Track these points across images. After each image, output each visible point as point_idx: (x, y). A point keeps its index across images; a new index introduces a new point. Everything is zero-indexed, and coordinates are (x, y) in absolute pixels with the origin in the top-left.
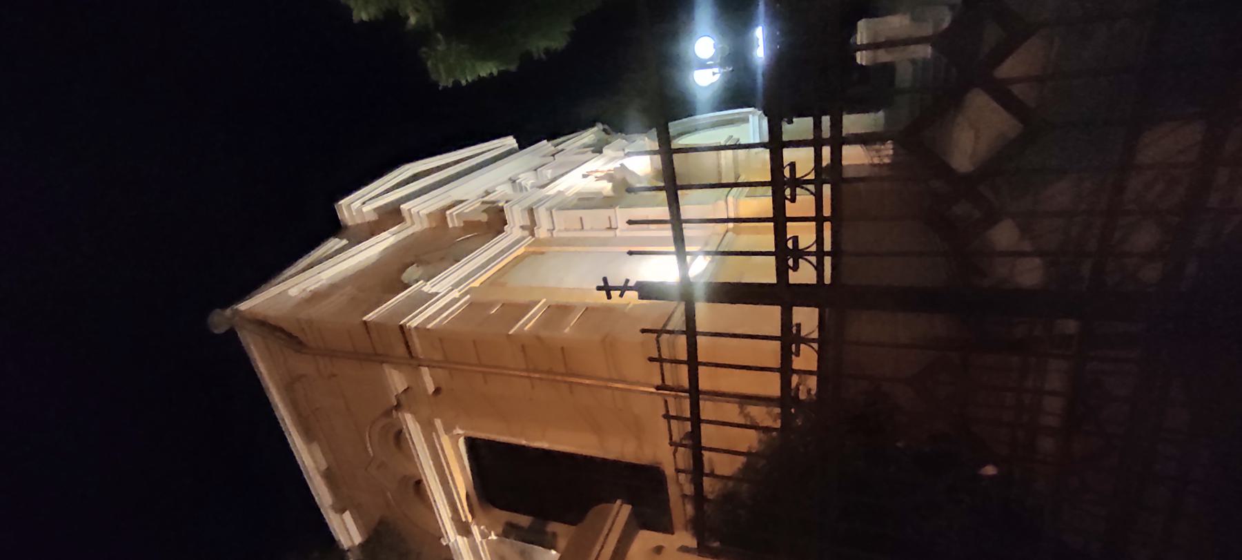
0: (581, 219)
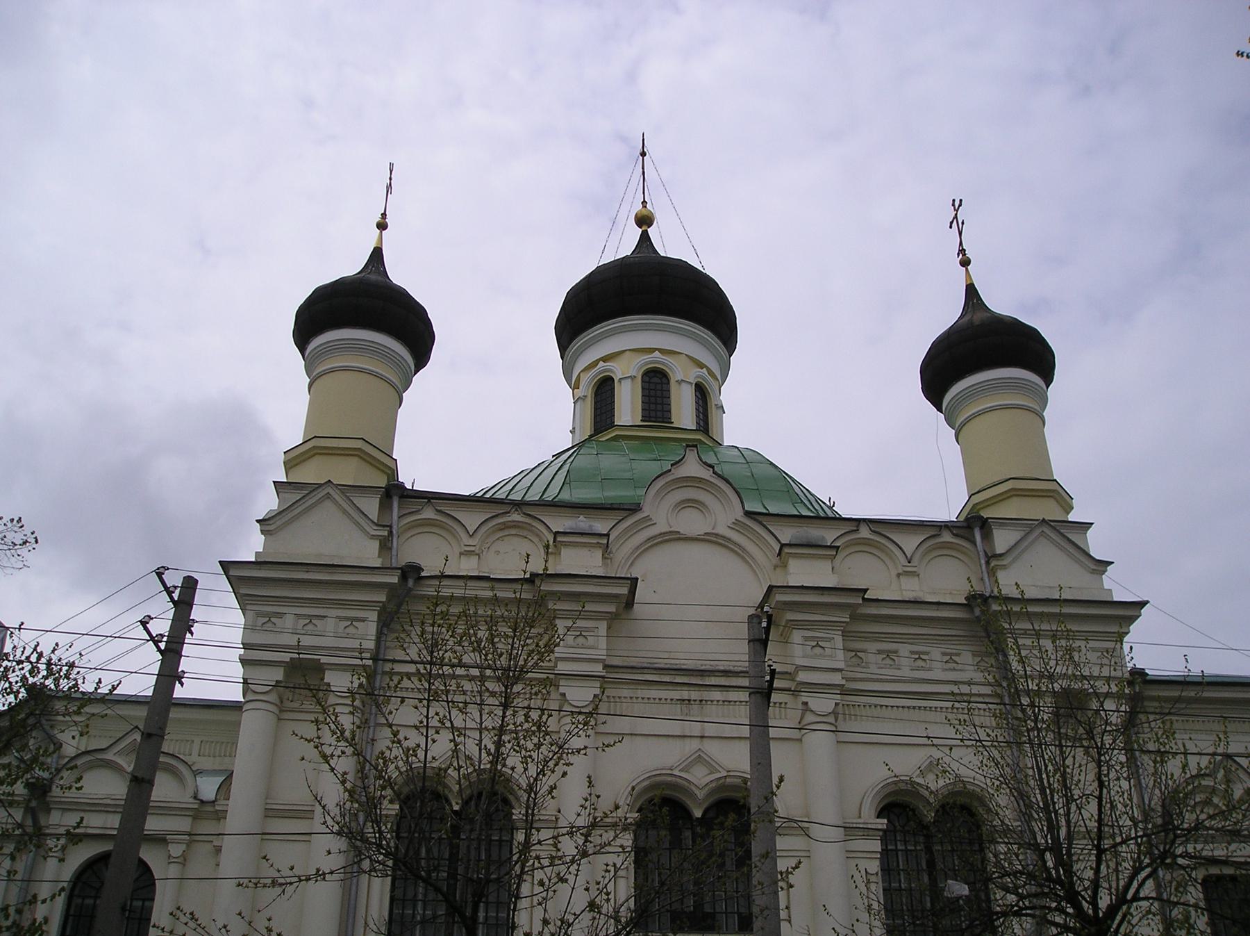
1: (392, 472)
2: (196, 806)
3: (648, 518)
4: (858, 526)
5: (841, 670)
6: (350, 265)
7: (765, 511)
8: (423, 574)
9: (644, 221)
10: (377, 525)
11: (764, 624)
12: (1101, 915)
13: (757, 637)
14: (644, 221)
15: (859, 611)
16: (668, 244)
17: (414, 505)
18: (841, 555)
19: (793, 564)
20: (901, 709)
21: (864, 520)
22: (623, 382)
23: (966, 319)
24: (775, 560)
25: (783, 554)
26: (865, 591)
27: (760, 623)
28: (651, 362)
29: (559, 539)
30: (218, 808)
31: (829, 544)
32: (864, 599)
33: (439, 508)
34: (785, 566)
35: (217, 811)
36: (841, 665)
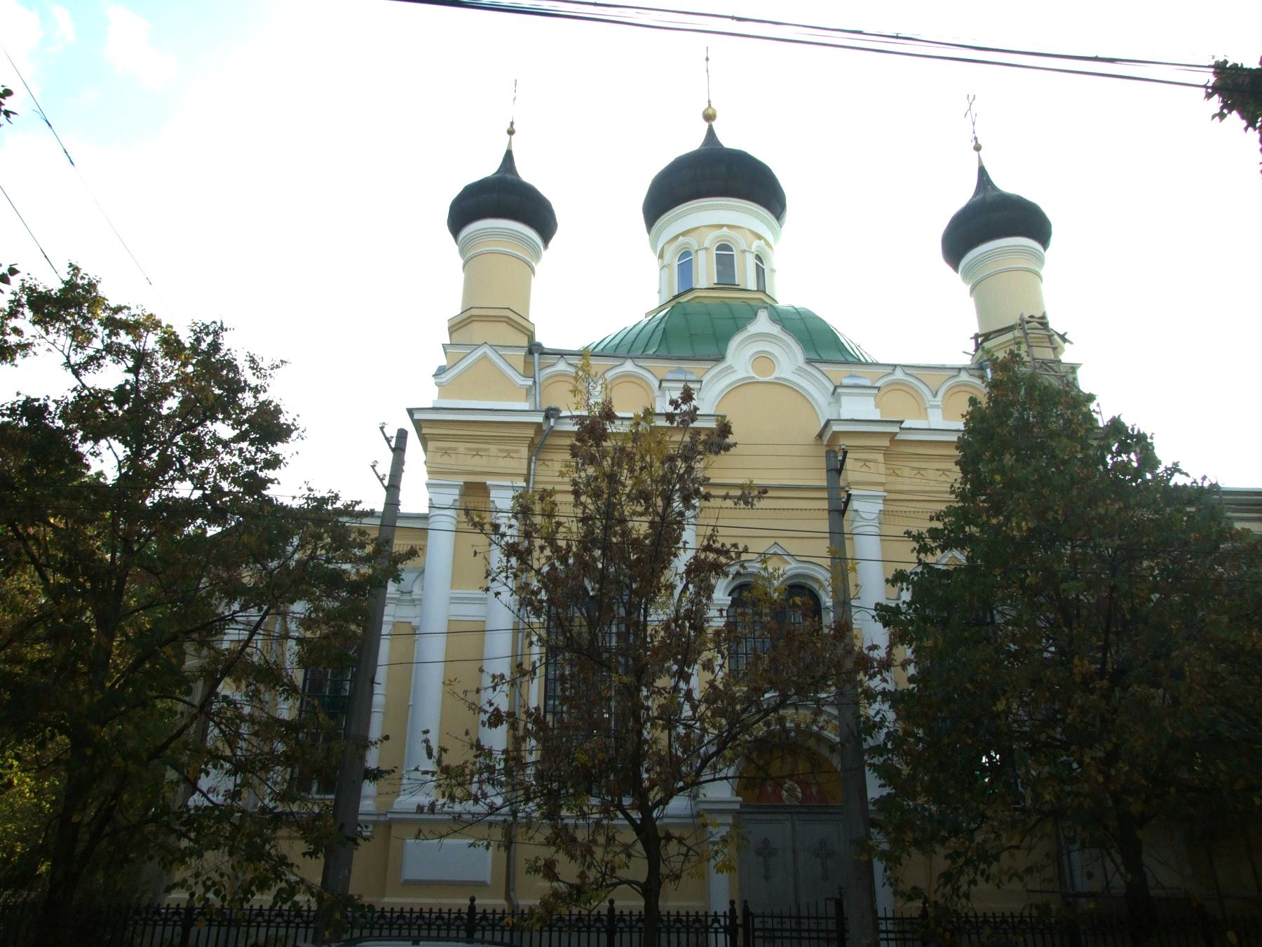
0: (516, 81)
1: (531, 335)
2: (398, 596)
3: (730, 367)
4: (894, 370)
5: (882, 484)
6: (488, 168)
7: (818, 358)
8: (561, 415)
9: (709, 117)
10: (524, 376)
11: (840, 458)
12: (639, 822)
13: (833, 468)
14: (709, 117)
15: (896, 438)
16: (729, 140)
17: (550, 359)
18: (882, 392)
19: (845, 400)
20: (278, 362)
21: (900, 365)
22: (699, 252)
23: (979, 197)
24: (830, 399)
25: (836, 394)
26: (902, 422)
27: (837, 457)
28: (722, 240)
29: (664, 384)
30: (414, 597)
31: (677, 293)
32: (900, 428)
33: (571, 362)
34: (838, 401)
35: (413, 600)
36: (882, 479)
